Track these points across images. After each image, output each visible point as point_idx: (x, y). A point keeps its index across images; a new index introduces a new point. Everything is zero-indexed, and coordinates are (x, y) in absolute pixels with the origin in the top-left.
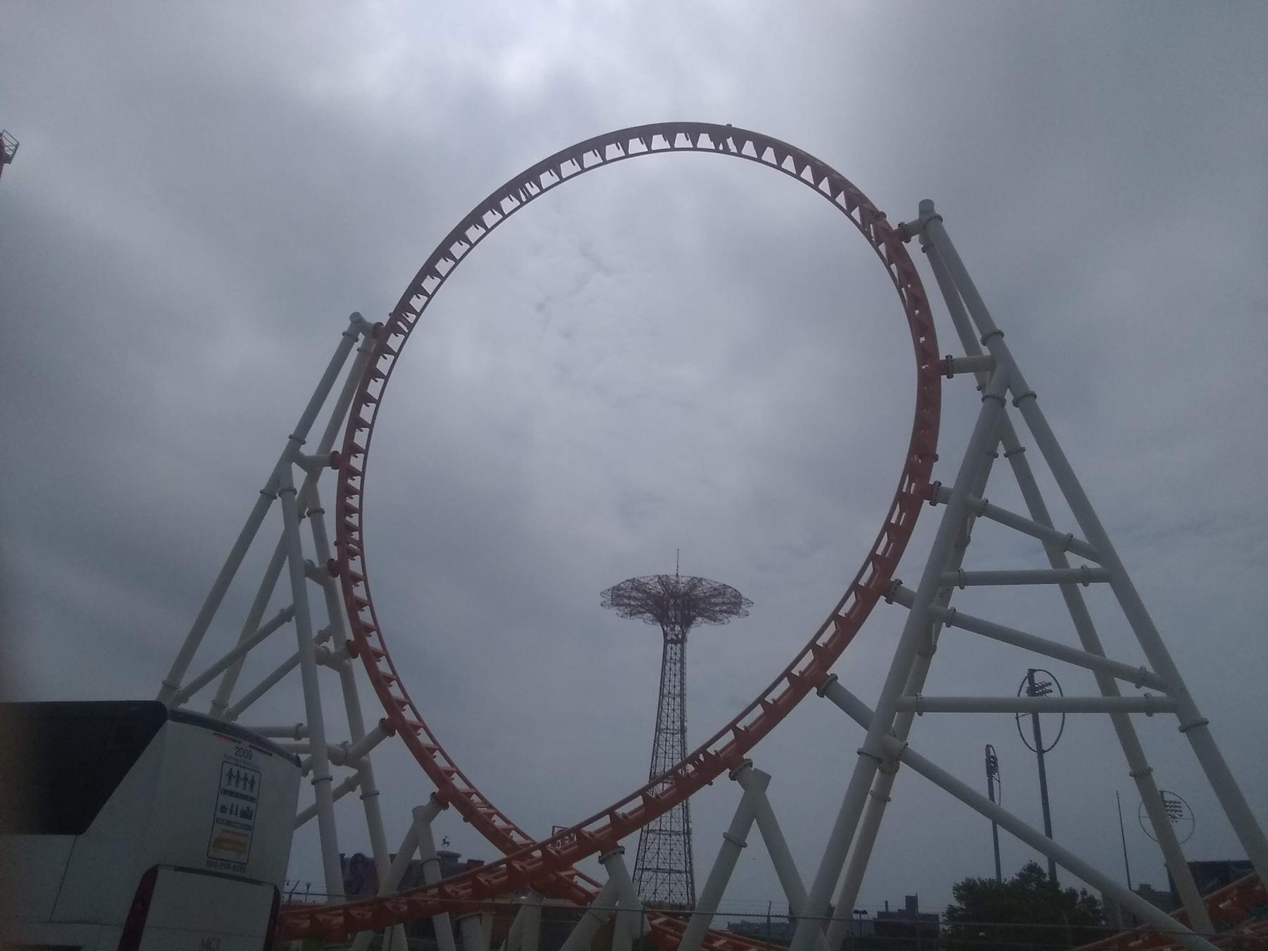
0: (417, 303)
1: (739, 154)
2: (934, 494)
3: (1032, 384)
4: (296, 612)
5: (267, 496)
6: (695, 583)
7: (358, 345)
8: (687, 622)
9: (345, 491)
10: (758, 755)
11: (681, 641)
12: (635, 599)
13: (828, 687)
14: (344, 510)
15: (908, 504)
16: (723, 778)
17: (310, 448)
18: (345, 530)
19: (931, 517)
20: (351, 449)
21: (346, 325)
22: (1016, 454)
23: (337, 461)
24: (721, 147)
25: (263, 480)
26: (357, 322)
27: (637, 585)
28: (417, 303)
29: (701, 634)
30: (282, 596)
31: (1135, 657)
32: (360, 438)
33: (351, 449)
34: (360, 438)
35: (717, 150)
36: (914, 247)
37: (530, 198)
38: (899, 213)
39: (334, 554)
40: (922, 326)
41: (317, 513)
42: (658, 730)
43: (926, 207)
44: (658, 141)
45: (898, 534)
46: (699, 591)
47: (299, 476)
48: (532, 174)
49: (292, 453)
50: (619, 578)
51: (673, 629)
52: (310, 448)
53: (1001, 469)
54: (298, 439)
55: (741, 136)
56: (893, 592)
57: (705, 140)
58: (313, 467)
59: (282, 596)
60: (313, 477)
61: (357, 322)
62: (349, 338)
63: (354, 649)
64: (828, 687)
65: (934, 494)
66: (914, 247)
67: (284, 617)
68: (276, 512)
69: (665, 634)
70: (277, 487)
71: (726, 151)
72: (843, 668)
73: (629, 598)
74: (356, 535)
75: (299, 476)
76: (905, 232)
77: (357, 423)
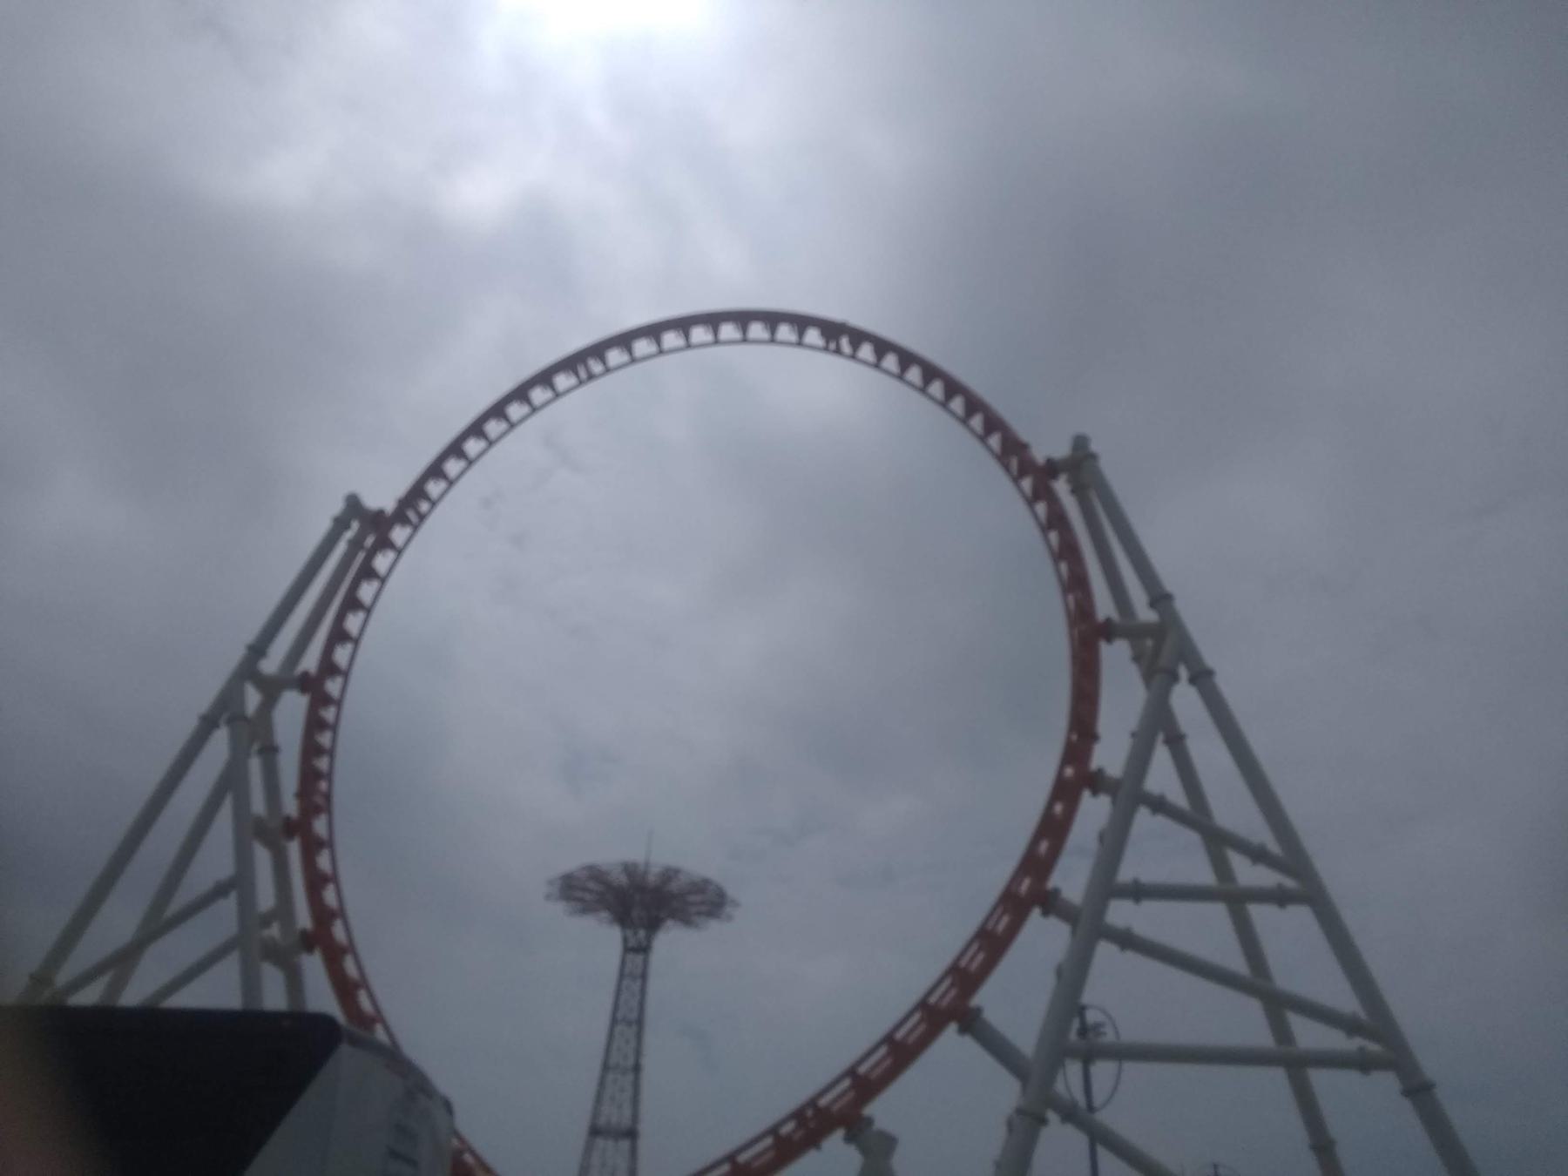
0: (434, 488)
1: (853, 357)
2: (1097, 782)
3: (1210, 658)
4: (239, 883)
5: (208, 724)
6: (670, 874)
7: (349, 535)
8: (653, 925)
9: (315, 724)
10: (882, 1111)
11: (644, 949)
12: (590, 891)
13: (970, 1022)
14: (311, 750)
15: (1066, 792)
16: (835, 1142)
17: (271, 664)
18: (310, 778)
19: (1094, 811)
20: (328, 668)
21: (337, 507)
22: (1176, 742)
23: (308, 684)
24: (832, 346)
25: (205, 697)
26: (353, 505)
27: (596, 874)
28: (434, 488)
29: (671, 942)
30: (216, 860)
31: (1340, 996)
32: (341, 655)
33: (328, 668)
34: (341, 655)
35: (826, 349)
36: (1061, 487)
37: (591, 377)
38: (1048, 445)
39: (291, 807)
40: (1076, 584)
41: (270, 752)
42: (606, 1067)
43: (1080, 443)
44: (785, 332)
45: (1053, 829)
46: (674, 886)
47: (253, 698)
48: (598, 350)
49: (248, 670)
50: (572, 861)
51: (635, 934)
52: (271, 664)
53: (1162, 757)
54: (258, 649)
55: (858, 337)
56: (1050, 903)
57: (813, 336)
58: (271, 689)
59: (216, 860)
60: (270, 701)
61: (353, 505)
62: (340, 524)
63: (308, 942)
64: (970, 1022)
65: (1097, 782)
66: (1061, 487)
67: (220, 891)
68: (219, 745)
69: (625, 940)
70: (224, 710)
71: (838, 351)
72: (990, 999)
73: (585, 889)
74: (323, 785)
75: (253, 698)
76: (1052, 469)
77: (339, 635)
